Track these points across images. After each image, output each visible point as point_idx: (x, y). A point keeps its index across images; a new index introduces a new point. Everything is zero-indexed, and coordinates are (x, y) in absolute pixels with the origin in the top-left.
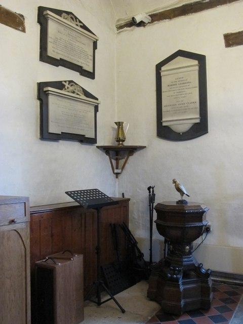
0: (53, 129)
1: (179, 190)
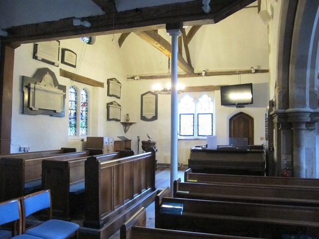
0: (111, 117)
1: (149, 137)
